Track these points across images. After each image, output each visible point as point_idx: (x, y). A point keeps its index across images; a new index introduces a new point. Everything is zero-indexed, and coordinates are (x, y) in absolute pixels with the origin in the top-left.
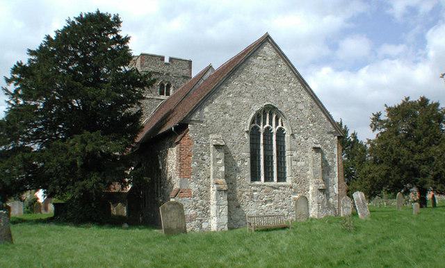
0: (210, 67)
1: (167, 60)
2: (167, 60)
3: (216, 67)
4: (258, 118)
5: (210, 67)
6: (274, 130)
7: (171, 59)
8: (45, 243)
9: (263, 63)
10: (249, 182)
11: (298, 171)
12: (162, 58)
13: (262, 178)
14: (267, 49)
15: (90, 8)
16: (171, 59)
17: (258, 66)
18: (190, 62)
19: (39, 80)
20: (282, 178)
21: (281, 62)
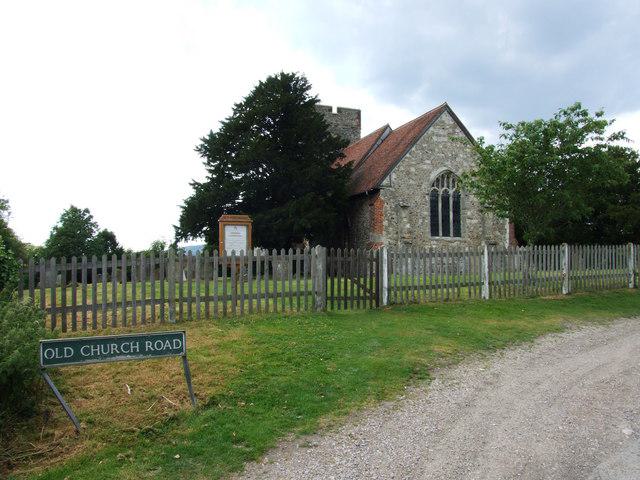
0: (388, 126)
1: (335, 111)
2: (335, 111)
3: (394, 127)
4: (438, 181)
5: (388, 126)
6: (451, 192)
7: (339, 110)
8: (268, 295)
9: (441, 132)
10: (430, 237)
11: (587, 342)
12: (330, 109)
13: (441, 234)
14: (445, 117)
15: (274, 71)
16: (339, 110)
17: (437, 134)
18: (358, 113)
19: (564, 292)
20: (457, 233)
21: (458, 130)
